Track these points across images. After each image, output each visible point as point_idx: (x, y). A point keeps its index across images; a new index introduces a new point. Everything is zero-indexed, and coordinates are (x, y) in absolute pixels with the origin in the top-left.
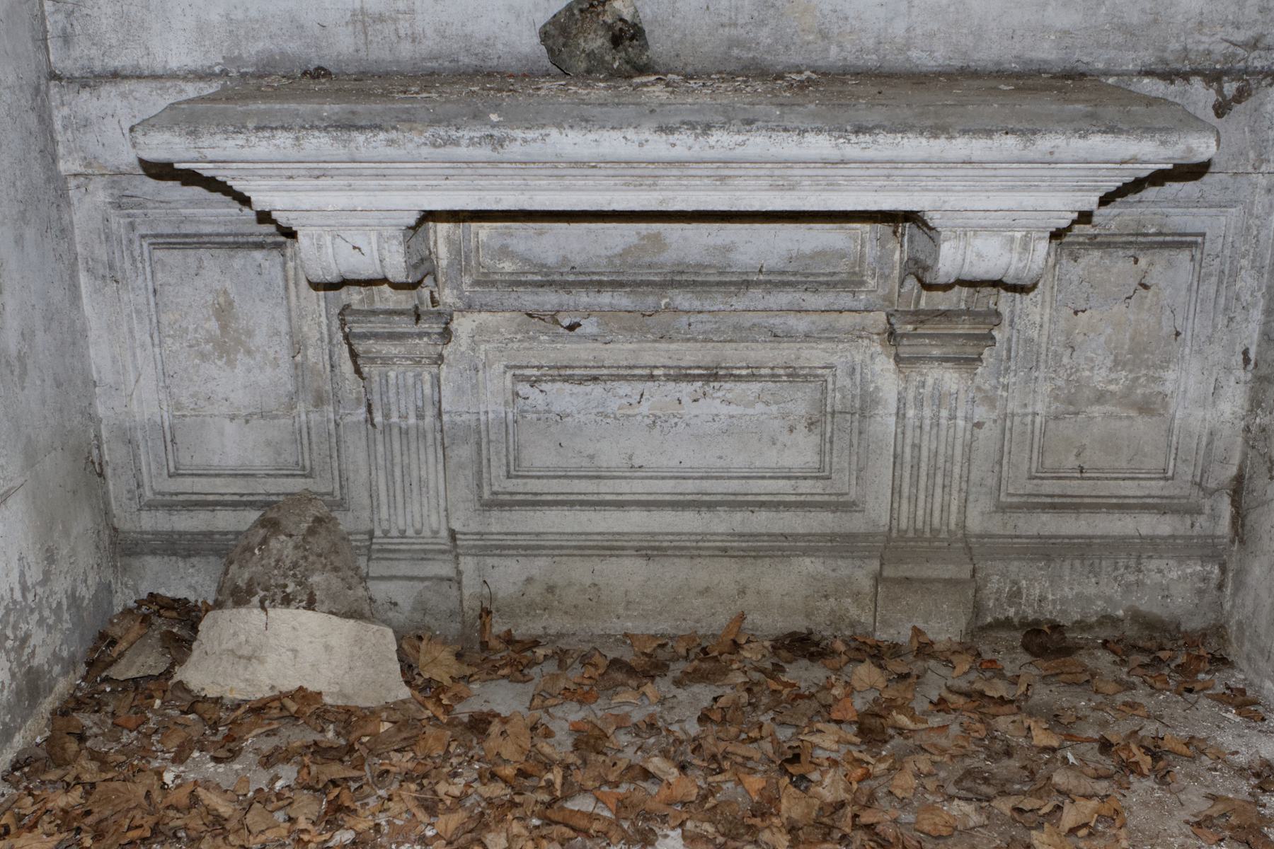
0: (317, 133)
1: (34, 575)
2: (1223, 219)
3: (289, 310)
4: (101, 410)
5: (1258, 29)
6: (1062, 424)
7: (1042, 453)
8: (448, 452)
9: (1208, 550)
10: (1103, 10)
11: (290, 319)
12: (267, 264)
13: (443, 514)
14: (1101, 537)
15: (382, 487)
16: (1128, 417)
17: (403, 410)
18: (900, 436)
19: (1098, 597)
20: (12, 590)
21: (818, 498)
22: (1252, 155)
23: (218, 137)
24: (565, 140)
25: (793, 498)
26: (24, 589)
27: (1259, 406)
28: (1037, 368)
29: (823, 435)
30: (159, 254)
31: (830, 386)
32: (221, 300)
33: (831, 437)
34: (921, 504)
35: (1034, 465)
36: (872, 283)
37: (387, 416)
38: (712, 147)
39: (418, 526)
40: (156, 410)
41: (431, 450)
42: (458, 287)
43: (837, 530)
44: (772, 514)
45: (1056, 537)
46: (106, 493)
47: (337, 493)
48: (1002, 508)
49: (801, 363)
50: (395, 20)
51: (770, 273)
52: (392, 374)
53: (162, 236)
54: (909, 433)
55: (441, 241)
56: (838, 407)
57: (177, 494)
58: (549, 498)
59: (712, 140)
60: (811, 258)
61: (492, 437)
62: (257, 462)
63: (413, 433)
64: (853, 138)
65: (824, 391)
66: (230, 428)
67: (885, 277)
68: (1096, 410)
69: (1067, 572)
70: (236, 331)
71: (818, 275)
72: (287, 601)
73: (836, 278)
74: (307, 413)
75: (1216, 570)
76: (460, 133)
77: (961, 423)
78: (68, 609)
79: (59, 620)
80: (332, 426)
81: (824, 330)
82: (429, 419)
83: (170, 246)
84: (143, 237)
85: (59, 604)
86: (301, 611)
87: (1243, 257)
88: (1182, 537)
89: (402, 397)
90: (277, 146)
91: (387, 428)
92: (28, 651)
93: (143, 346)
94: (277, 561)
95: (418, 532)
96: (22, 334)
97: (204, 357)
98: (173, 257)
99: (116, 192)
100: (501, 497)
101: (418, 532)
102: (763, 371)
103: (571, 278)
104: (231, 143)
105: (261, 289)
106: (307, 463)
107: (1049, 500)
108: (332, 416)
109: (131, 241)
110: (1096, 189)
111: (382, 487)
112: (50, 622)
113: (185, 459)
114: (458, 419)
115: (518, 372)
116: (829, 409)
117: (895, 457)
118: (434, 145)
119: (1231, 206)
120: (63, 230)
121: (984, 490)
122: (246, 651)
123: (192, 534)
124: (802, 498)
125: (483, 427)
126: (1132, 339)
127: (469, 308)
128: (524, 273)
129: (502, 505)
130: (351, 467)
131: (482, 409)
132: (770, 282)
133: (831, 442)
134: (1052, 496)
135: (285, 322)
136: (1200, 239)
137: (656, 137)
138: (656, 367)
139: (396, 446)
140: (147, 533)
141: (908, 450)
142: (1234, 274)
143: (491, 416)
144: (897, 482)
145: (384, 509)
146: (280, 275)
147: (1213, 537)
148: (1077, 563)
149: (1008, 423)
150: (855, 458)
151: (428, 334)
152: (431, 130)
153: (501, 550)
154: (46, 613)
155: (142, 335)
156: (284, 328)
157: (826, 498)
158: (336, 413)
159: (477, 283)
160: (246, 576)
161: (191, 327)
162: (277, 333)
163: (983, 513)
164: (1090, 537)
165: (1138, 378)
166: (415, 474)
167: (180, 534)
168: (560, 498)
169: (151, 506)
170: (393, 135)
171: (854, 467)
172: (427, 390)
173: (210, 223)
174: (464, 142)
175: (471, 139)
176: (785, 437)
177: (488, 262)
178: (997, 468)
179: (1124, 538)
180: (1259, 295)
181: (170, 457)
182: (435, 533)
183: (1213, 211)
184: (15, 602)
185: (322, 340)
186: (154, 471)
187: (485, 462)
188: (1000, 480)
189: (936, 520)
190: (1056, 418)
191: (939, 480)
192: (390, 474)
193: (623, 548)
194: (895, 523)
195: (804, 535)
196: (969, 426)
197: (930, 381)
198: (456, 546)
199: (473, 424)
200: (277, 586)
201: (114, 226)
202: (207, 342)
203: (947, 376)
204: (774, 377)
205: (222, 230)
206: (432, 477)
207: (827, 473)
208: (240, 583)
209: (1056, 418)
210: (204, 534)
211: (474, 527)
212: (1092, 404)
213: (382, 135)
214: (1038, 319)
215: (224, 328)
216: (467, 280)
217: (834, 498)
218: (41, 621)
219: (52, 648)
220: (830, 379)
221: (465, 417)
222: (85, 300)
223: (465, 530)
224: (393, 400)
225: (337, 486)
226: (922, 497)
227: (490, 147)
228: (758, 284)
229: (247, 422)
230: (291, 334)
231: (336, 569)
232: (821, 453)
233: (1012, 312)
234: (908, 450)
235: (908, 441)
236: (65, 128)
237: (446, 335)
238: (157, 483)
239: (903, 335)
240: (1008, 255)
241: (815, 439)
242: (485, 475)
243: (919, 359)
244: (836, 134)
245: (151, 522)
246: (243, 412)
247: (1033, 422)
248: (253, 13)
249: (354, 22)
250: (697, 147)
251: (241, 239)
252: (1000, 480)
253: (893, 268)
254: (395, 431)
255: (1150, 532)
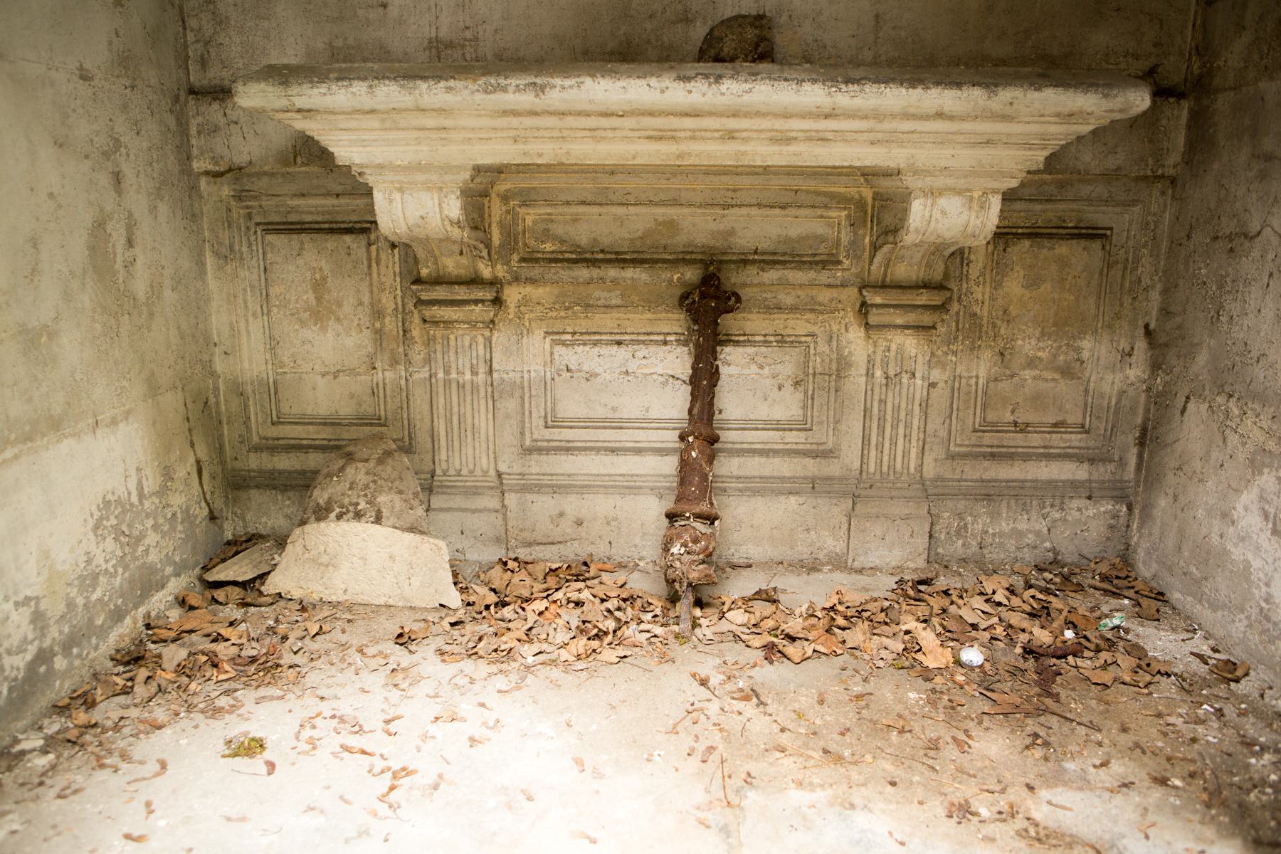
0: (387, 82)
1: (151, 484)
2: (1126, 216)
3: (371, 285)
4: (219, 366)
5: (1153, 60)
6: (1001, 385)
7: (984, 408)
8: (498, 405)
9: (1120, 494)
10: (1030, 43)
11: (371, 292)
12: (355, 246)
13: (492, 456)
14: (1032, 481)
15: (443, 433)
16: (1053, 379)
17: (460, 366)
18: (869, 393)
19: (1029, 531)
20: (129, 494)
21: (801, 447)
22: (1150, 161)
23: (305, 86)
24: (597, 86)
25: (781, 447)
26: (141, 496)
27: (1160, 368)
28: (980, 338)
29: (806, 392)
30: (269, 238)
31: (812, 352)
32: (317, 276)
33: (813, 395)
34: (886, 451)
35: (978, 420)
36: (847, 263)
37: (447, 372)
38: (723, 94)
39: (471, 467)
40: (264, 368)
41: (483, 402)
42: (507, 263)
43: (817, 473)
44: (763, 460)
45: (996, 481)
46: (221, 436)
47: (406, 439)
48: (952, 457)
49: (789, 331)
50: (463, 47)
51: (763, 253)
52: (452, 337)
53: (272, 223)
54: (877, 391)
55: (494, 225)
56: (819, 370)
57: (278, 439)
58: (580, 444)
59: (723, 88)
60: (798, 242)
61: (533, 393)
62: (342, 412)
63: (468, 387)
64: (843, 87)
65: (807, 355)
66: (321, 382)
67: (858, 258)
68: (1027, 374)
69: (1005, 510)
70: (328, 302)
71: (802, 256)
72: (358, 516)
73: (817, 258)
74: (384, 370)
75: (1125, 509)
76: (508, 81)
77: (919, 382)
78: (182, 522)
79: (173, 529)
80: (403, 382)
81: (806, 304)
82: (481, 377)
83: (278, 232)
84: (258, 224)
85: (174, 515)
86: (370, 525)
87: (1144, 247)
88: (1096, 481)
89: (460, 356)
90: (354, 94)
91: (447, 383)
92: (141, 548)
93: (254, 315)
94: (352, 483)
95: (471, 472)
96: (152, 286)
97: (303, 323)
98: (278, 240)
99: (237, 187)
100: (539, 444)
101: (471, 472)
102: (757, 338)
103: (601, 256)
104: (315, 91)
105: (349, 266)
106: (383, 413)
107: (989, 450)
108: (403, 373)
109: (248, 228)
110: (1044, 148)
111: (443, 433)
112: (166, 528)
113: (285, 409)
114: (505, 376)
115: (557, 337)
116: (811, 371)
117: (865, 411)
118: (486, 92)
119: (1134, 205)
120: (193, 215)
121: (937, 440)
122: (325, 559)
123: (290, 472)
124: (788, 447)
125: (526, 384)
126: (1056, 315)
127: (516, 279)
128: (562, 252)
129: (540, 450)
130: (418, 417)
131: (526, 369)
132: (763, 261)
133: (813, 399)
134: (992, 447)
135: (368, 294)
136: (1108, 233)
137: (675, 84)
138: (669, 334)
139: (455, 398)
140: (253, 471)
141: (876, 405)
142: (1137, 260)
143: (533, 374)
144: (867, 432)
145: (443, 452)
146: (365, 255)
147: (1121, 481)
148: (1013, 503)
149: (957, 385)
150: (832, 413)
151: (482, 301)
152: (484, 79)
153: (538, 488)
154: (161, 521)
155: (254, 305)
156: (366, 300)
157: (808, 447)
158: (406, 370)
159: (523, 260)
160: (326, 497)
161: (293, 298)
162: (361, 304)
163: (936, 460)
164: (1022, 481)
165: (1060, 347)
166: (469, 422)
167: (281, 472)
168: (589, 444)
169: (257, 449)
170: (452, 83)
171: (831, 420)
172: (481, 352)
173: (311, 213)
174: (511, 89)
175: (517, 86)
176: (775, 394)
177: (532, 243)
178: (948, 421)
179: (1050, 482)
180: (1156, 278)
181: (273, 407)
182: (485, 473)
183: (1119, 209)
184: (132, 505)
185: (396, 309)
186: (260, 420)
187: (527, 413)
188: (950, 431)
189: (899, 465)
190: (996, 380)
191: (901, 431)
192: (449, 421)
193: (640, 488)
194: (865, 467)
195: (790, 478)
196: (926, 384)
197: (894, 347)
198: (501, 483)
199: (518, 381)
200: (351, 504)
201: (235, 216)
202: (305, 311)
203: (908, 342)
204: (766, 343)
205: (320, 219)
206: (483, 425)
207: (808, 426)
208: (321, 501)
209: (996, 380)
210: (297, 472)
211: (517, 468)
212: (1024, 369)
213: (443, 84)
214: (980, 297)
215: (319, 299)
216: (515, 257)
217: (814, 447)
218: (155, 527)
219: (165, 551)
220: (812, 346)
221: (511, 375)
222: (210, 276)
223: (509, 471)
224: (452, 359)
225: (406, 433)
226: (887, 445)
227: (533, 94)
228: (753, 262)
229: (335, 377)
230: (372, 304)
231: (400, 492)
232: (804, 407)
233: (959, 290)
234: (876, 405)
235: (876, 397)
236: (199, 133)
237: (497, 301)
238: (260, 429)
239: (873, 305)
240: (966, 213)
241: (800, 396)
242: (527, 425)
243: (884, 326)
244: (830, 84)
245: (255, 462)
246: (333, 369)
247: (977, 383)
248: (351, 41)
249: (430, 48)
250: (710, 94)
251: (334, 226)
252: (950, 431)
253: (864, 250)
254: (454, 386)
255: (1071, 477)
